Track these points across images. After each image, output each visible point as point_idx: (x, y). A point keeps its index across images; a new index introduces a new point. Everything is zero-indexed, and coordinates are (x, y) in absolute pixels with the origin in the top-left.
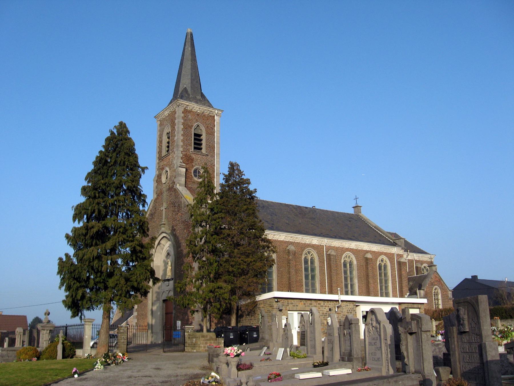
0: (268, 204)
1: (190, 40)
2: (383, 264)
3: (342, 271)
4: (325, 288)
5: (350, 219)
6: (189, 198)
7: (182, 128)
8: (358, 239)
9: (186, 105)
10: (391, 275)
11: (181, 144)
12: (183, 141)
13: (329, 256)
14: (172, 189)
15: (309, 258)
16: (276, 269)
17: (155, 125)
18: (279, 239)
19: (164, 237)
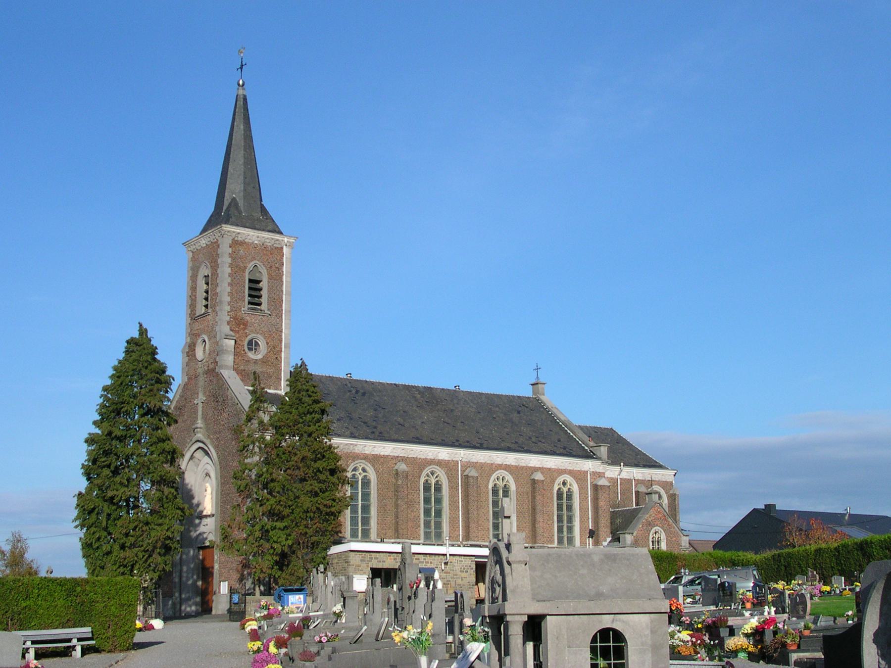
0: (373, 388)
1: (242, 109)
2: (565, 490)
3: (488, 502)
4: (457, 529)
5: (520, 409)
6: (242, 393)
7: (229, 273)
8: (523, 448)
9: (234, 234)
10: (580, 507)
11: (228, 299)
12: (231, 294)
13: (466, 478)
14: (213, 373)
15: (433, 481)
16: (376, 501)
17: (184, 258)
18: (382, 454)
19: (200, 448)
